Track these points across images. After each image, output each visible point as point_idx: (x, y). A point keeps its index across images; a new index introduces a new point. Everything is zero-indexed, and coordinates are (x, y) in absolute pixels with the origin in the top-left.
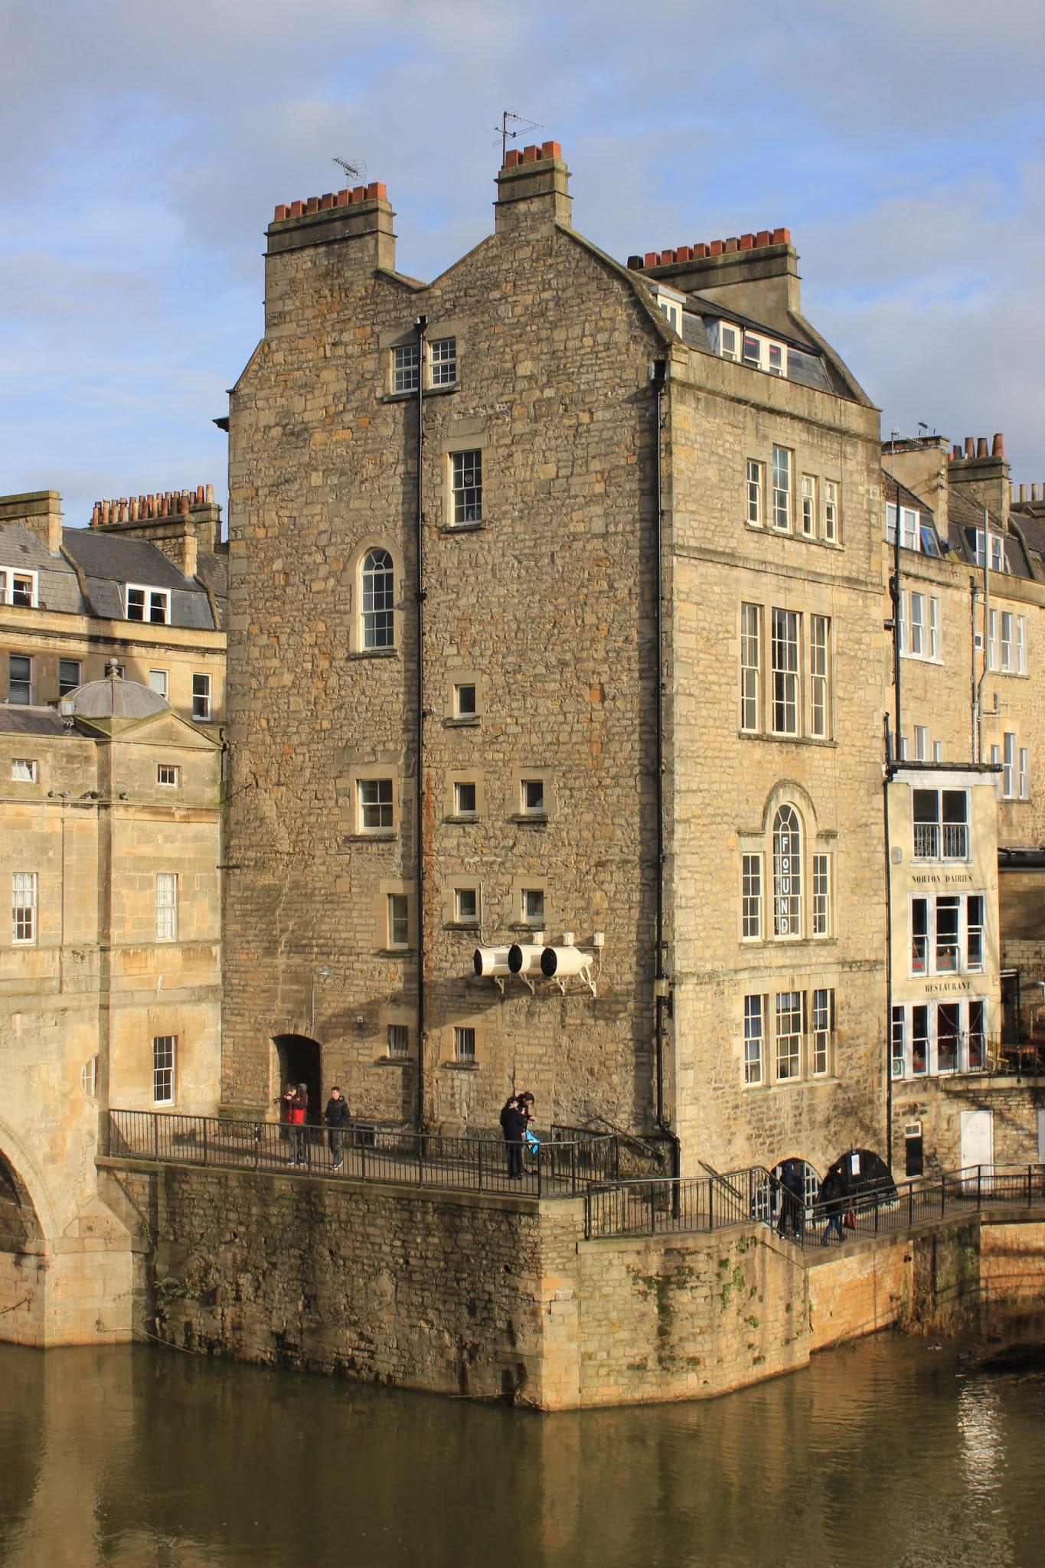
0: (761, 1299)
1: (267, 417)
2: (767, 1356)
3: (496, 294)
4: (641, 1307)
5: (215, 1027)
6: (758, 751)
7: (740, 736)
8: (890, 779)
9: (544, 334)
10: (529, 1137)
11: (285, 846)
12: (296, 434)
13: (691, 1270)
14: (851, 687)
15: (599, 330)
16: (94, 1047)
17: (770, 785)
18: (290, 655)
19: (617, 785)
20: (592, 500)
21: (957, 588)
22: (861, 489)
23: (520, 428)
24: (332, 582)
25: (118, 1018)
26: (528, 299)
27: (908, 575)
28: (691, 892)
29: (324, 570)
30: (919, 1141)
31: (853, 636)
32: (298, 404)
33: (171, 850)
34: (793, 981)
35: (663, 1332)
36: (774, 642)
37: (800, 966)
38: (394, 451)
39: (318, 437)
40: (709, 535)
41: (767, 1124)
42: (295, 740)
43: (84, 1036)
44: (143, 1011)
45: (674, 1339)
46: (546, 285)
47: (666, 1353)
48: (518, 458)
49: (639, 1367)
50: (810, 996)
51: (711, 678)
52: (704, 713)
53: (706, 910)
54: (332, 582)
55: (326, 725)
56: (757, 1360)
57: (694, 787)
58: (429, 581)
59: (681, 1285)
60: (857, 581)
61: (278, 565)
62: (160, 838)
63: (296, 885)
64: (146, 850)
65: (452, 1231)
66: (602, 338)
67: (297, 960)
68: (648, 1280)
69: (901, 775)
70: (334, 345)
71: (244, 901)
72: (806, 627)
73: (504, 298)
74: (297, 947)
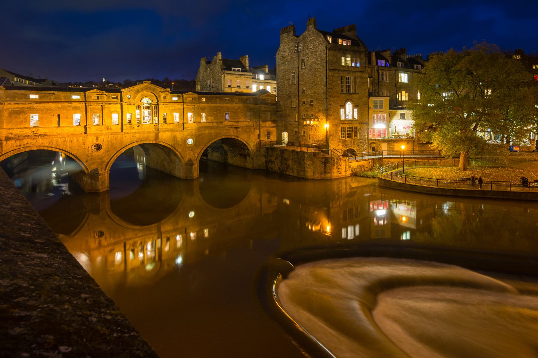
0: (341, 166)
1: (280, 56)
2: (342, 173)
3: (307, 38)
4: (322, 165)
5: (275, 131)
6: (344, 96)
7: (340, 93)
8: (368, 99)
9: (312, 43)
10: (247, 152)
11: (283, 109)
12: (284, 58)
13: (329, 161)
14: (361, 86)
15: (319, 42)
16: (258, 133)
17: (346, 100)
18: (284, 85)
19: (322, 100)
20: (319, 64)
21: (392, 71)
22: (364, 59)
23: (310, 55)
24: (288, 76)
25: (262, 130)
26: (311, 38)
27: (381, 70)
28: (331, 114)
29: (287, 74)
30: (374, 147)
31: (362, 79)
32: (284, 54)
33: (269, 109)
34: (350, 125)
35: (325, 169)
36: (347, 81)
37: (239, 122)
38: (296, 59)
39: (286, 58)
40: (335, 67)
41: (345, 144)
42: (284, 96)
43: (257, 132)
44: (265, 129)
45: (327, 169)
46: (312, 36)
47: (325, 171)
48: (310, 59)
49: (322, 173)
50: (353, 128)
51: (335, 86)
52: (334, 91)
53: (334, 116)
54: (288, 76)
55: (288, 94)
56: (340, 173)
57: (332, 100)
58: (299, 75)
59: (327, 163)
60: (363, 72)
61: (282, 74)
62: (267, 108)
63: (285, 113)
64: (266, 109)
65: (297, 155)
66: (319, 43)
67: (285, 123)
68: (323, 162)
69: (371, 98)
70: (288, 46)
71: (279, 115)
72: (346, 128)
73: (308, 38)
74: (285, 121)
